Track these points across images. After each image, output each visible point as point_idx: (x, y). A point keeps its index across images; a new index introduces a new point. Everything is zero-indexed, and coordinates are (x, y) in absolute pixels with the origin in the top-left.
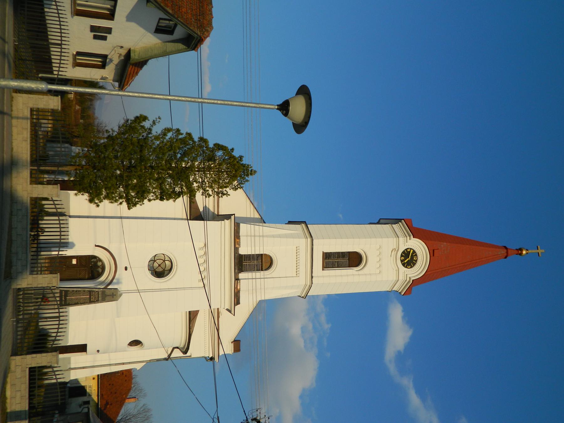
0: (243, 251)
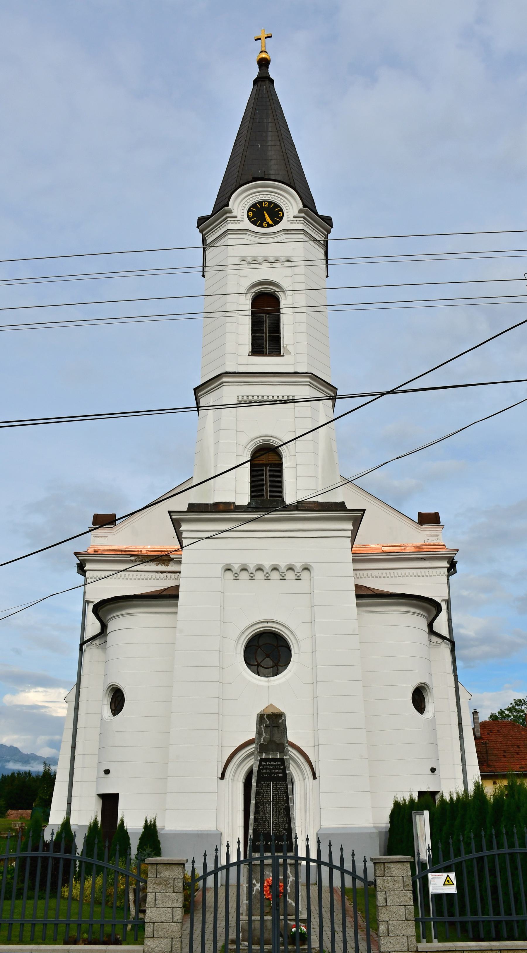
0: (243, 498)
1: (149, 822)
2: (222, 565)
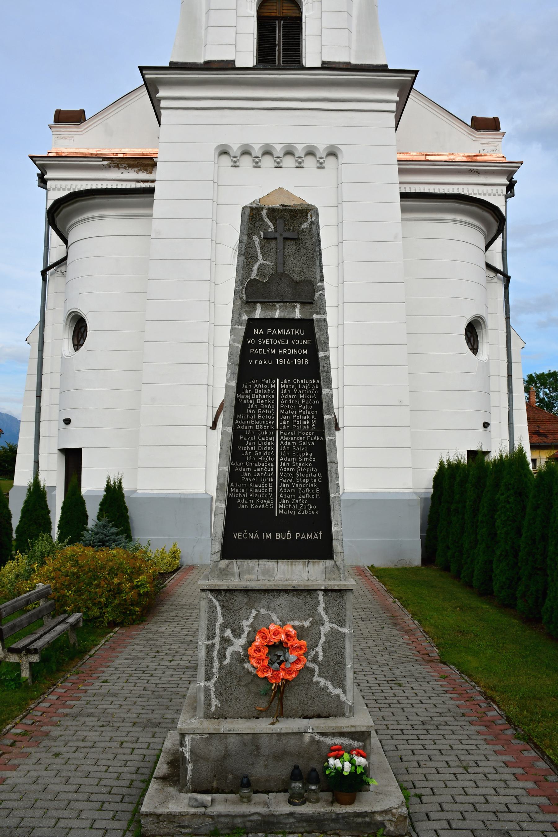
0: (247, 56)
1: (112, 482)
2: (216, 145)
